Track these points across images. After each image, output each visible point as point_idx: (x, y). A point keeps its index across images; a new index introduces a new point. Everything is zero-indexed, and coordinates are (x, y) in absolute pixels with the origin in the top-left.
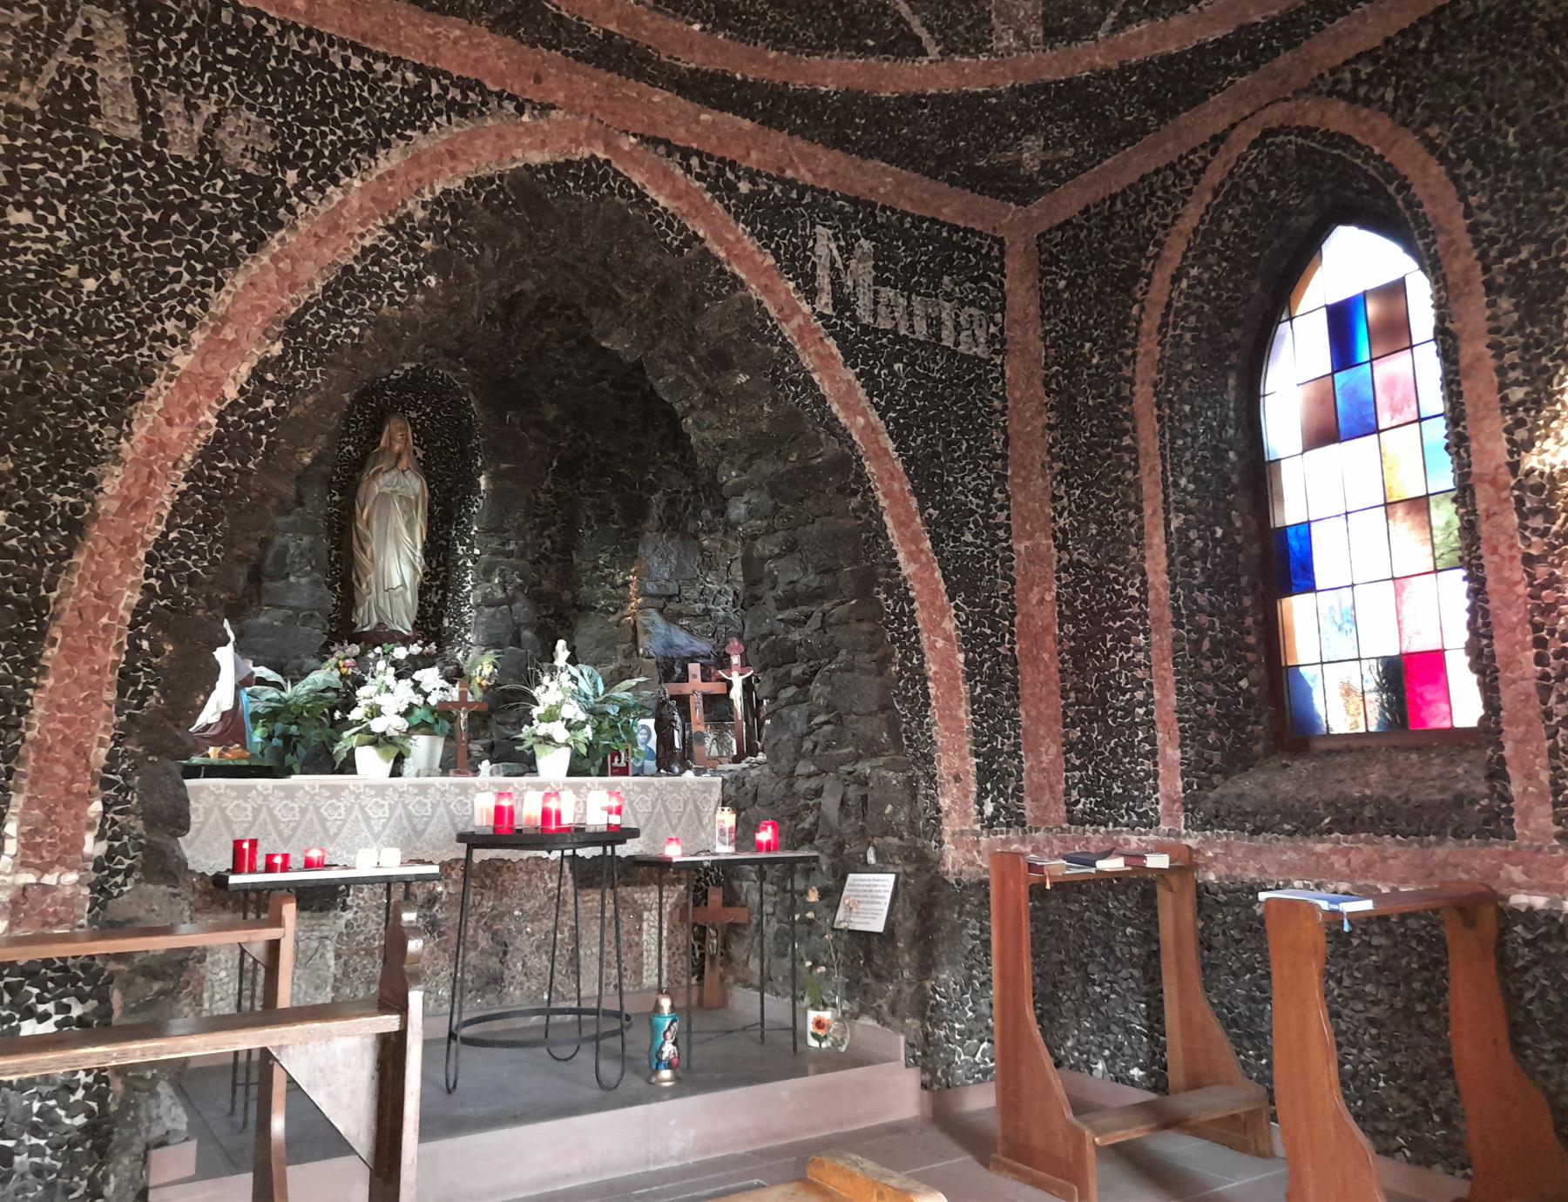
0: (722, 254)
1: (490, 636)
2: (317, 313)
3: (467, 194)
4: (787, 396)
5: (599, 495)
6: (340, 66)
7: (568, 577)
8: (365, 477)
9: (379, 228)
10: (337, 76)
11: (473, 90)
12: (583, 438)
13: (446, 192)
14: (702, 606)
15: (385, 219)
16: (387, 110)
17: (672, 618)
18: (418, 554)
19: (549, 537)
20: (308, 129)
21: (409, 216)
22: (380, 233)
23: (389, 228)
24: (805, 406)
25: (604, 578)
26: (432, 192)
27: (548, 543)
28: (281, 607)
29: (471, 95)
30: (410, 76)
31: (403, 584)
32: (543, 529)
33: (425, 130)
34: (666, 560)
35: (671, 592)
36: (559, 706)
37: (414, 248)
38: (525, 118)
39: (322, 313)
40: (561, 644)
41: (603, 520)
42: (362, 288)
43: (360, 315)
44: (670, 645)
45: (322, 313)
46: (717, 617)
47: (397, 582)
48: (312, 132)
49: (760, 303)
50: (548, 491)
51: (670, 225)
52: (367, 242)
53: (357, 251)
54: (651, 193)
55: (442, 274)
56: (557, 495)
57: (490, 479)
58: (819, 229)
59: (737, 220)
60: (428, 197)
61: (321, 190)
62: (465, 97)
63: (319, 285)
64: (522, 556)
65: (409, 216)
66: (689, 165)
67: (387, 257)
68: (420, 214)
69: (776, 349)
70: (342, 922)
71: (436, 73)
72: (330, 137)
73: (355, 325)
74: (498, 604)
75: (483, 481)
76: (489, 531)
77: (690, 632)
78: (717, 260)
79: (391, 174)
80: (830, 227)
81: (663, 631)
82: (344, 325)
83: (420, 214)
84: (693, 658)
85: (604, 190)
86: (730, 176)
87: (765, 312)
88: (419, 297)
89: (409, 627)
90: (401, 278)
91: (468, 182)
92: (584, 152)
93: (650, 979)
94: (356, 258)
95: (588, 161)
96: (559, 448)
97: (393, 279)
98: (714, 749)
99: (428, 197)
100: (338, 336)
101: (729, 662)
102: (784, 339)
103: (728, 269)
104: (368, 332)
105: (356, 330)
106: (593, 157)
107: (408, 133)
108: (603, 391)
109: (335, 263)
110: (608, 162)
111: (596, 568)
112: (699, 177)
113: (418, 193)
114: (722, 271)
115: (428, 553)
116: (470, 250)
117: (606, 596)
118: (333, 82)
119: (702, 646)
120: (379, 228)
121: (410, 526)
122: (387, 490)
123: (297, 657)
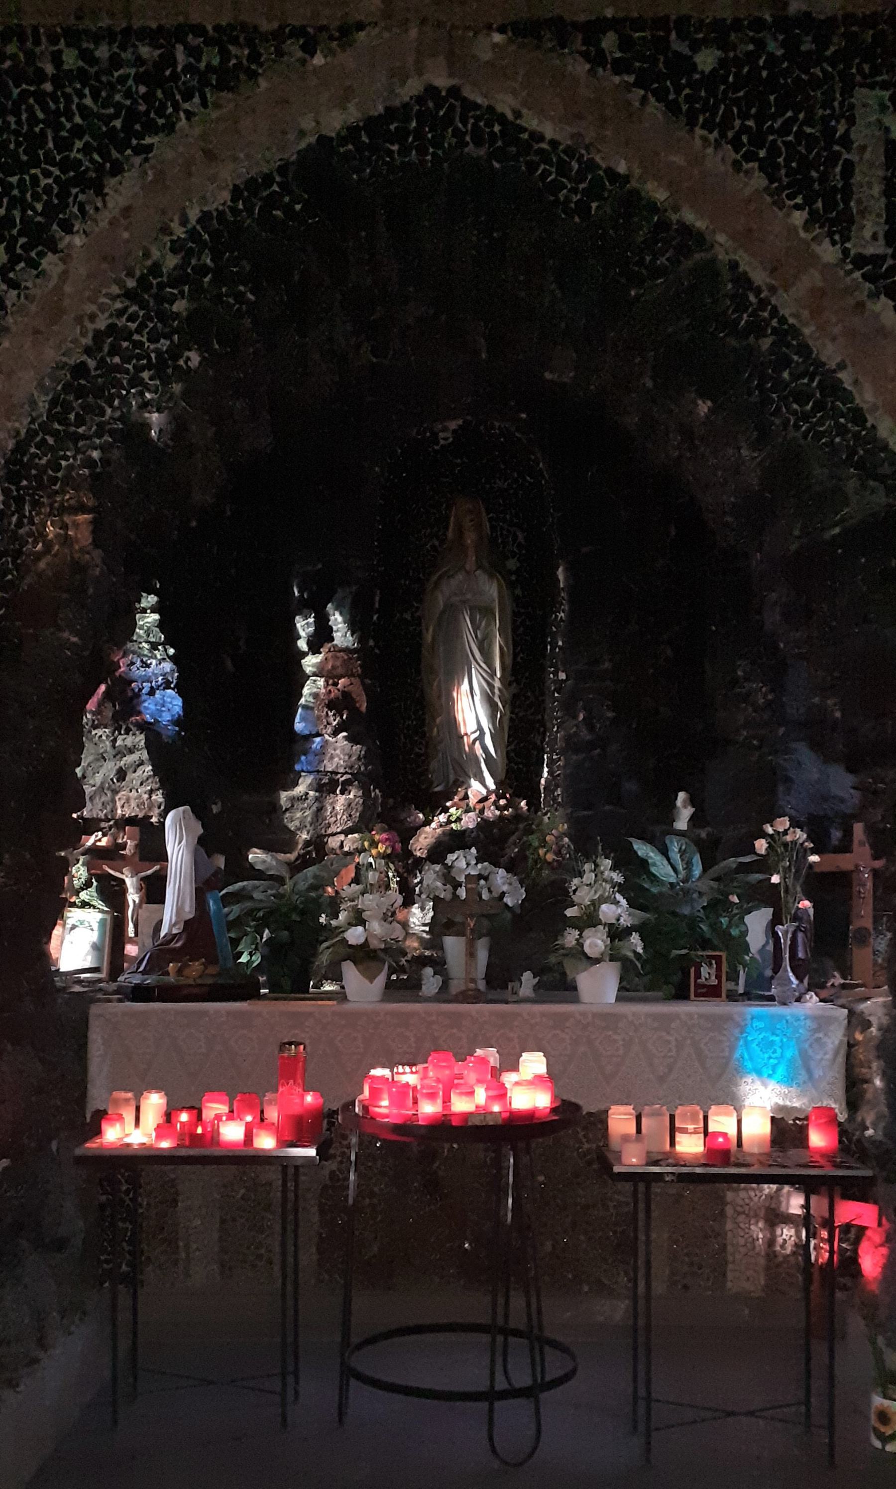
0: (661, 195)
2: (44, 440)
3: (234, 210)
4: (786, 424)
6: (49, 69)
9: (114, 298)
10: (48, 87)
11: (235, 41)
13: (205, 218)
15: (119, 282)
16: (116, 116)
18: (497, 684)
20: (14, 180)
21: (155, 269)
22: (118, 305)
23: (128, 295)
24: (819, 436)
26: (184, 222)
29: (233, 49)
30: (145, 51)
31: (480, 728)
33: (170, 128)
36: (595, 905)
37: (164, 317)
38: (318, 60)
39: (51, 441)
42: (99, 392)
45: (51, 441)
48: (21, 181)
49: (734, 265)
51: (563, 169)
52: (102, 323)
53: (87, 341)
54: (530, 121)
55: (204, 347)
58: (861, 94)
59: (691, 123)
60: (180, 232)
61: (34, 264)
62: (225, 55)
63: (43, 404)
65: (155, 269)
66: (601, 53)
67: (128, 338)
68: (172, 261)
69: (766, 343)
70: (326, 1172)
71: (179, 33)
72: (44, 182)
75: (561, 573)
78: (653, 207)
79: (127, 211)
80: (884, 86)
82: (78, 451)
83: (172, 261)
85: (450, 140)
86: (680, 47)
87: (743, 281)
88: (177, 388)
90: (149, 366)
91: (236, 193)
92: (413, 87)
94: (88, 351)
95: (420, 100)
97: (139, 369)
99: (180, 232)
100: (71, 467)
102: (783, 320)
103: (674, 217)
104: (116, 454)
105: (96, 454)
106: (431, 91)
107: (148, 140)
109: (61, 366)
110: (454, 91)
112: (619, 67)
113: (165, 230)
114: (663, 225)
116: (240, 297)
118: (40, 97)
120: (114, 298)
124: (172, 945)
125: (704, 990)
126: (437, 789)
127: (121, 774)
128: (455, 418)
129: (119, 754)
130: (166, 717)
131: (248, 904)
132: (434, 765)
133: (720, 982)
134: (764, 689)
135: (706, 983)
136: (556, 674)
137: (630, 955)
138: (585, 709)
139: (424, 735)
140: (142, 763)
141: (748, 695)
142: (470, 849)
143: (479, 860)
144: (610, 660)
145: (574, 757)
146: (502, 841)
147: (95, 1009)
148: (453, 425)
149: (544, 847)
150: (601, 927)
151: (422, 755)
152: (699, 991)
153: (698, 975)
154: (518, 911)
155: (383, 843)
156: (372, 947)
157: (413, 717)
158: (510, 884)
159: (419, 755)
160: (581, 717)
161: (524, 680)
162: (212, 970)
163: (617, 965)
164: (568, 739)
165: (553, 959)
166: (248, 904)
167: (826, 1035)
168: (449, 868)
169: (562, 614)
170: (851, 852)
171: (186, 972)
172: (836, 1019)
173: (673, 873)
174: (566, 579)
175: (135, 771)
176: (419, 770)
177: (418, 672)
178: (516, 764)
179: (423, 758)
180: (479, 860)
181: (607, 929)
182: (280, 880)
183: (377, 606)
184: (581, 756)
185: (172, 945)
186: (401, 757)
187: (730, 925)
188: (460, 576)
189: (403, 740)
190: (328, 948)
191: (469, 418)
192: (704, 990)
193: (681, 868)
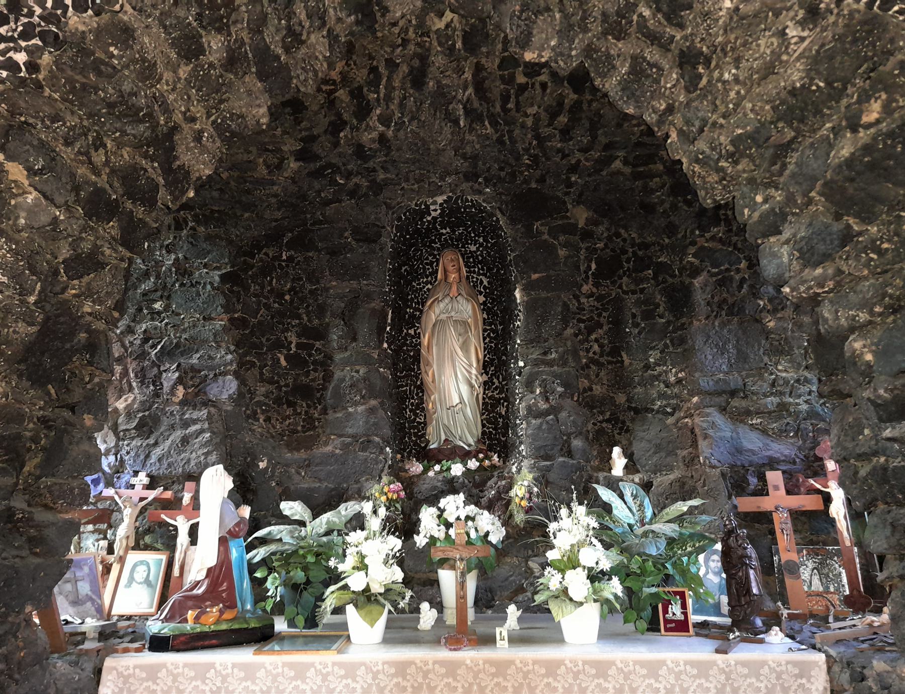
1: (538, 449)
5: (642, 291)
7: (621, 381)
12: (618, 235)
14: (775, 400)
17: (739, 417)
18: (474, 371)
19: (596, 340)
25: (657, 378)
27: (596, 347)
28: (340, 436)
31: (462, 401)
32: (590, 333)
34: (723, 351)
35: (732, 386)
40: (617, 451)
41: (648, 315)
43: (26, 34)
44: (739, 450)
46: (797, 414)
47: (456, 400)
50: (591, 295)
56: (599, 298)
57: (525, 290)
64: (565, 364)
73: (17, 49)
74: (546, 413)
75: (518, 294)
76: (531, 341)
77: (764, 432)
81: (728, 434)
84: (772, 464)
89: (471, 441)
93: (848, 543)
96: (596, 250)
98: (816, 581)
101: (823, 467)
105: (21, 58)
108: (619, 172)
111: (647, 367)
115: (485, 367)
117: (662, 396)
119: (782, 449)
121: (465, 347)
122: (443, 317)
123: (357, 482)
124: (195, 592)
125: (673, 625)
127: (185, 440)
128: (441, 194)
129: (186, 424)
130: (225, 396)
131: (273, 547)
132: (430, 429)
133: (685, 614)
134: (674, 370)
135: (673, 618)
136: (516, 362)
137: (611, 597)
138: (540, 386)
139: (423, 409)
140: (202, 431)
141: (660, 375)
143: (466, 503)
144: (556, 352)
145: (534, 421)
146: (481, 486)
147: (109, 662)
148: (440, 199)
150: (579, 570)
152: (669, 626)
153: (666, 611)
154: (500, 546)
156: (373, 591)
158: (493, 524)
159: (419, 423)
160: (538, 391)
162: (228, 615)
163: (598, 605)
164: (529, 408)
165: (539, 598)
166: (273, 547)
167: (809, 681)
168: (442, 511)
170: (767, 494)
171: (203, 619)
172: (815, 663)
173: (630, 515)
174: (521, 298)
175: (196, 438)
178: (488, 428)
180: (466, 503)
181: (586, 571)
182: (302, 524)
183: (389, 321)
184: (539, 421)
185: (195, 592)
187: (688, 564)
188: (447, 301)
190: (333, 592)
192: (673, 625)
193: (635, 511)
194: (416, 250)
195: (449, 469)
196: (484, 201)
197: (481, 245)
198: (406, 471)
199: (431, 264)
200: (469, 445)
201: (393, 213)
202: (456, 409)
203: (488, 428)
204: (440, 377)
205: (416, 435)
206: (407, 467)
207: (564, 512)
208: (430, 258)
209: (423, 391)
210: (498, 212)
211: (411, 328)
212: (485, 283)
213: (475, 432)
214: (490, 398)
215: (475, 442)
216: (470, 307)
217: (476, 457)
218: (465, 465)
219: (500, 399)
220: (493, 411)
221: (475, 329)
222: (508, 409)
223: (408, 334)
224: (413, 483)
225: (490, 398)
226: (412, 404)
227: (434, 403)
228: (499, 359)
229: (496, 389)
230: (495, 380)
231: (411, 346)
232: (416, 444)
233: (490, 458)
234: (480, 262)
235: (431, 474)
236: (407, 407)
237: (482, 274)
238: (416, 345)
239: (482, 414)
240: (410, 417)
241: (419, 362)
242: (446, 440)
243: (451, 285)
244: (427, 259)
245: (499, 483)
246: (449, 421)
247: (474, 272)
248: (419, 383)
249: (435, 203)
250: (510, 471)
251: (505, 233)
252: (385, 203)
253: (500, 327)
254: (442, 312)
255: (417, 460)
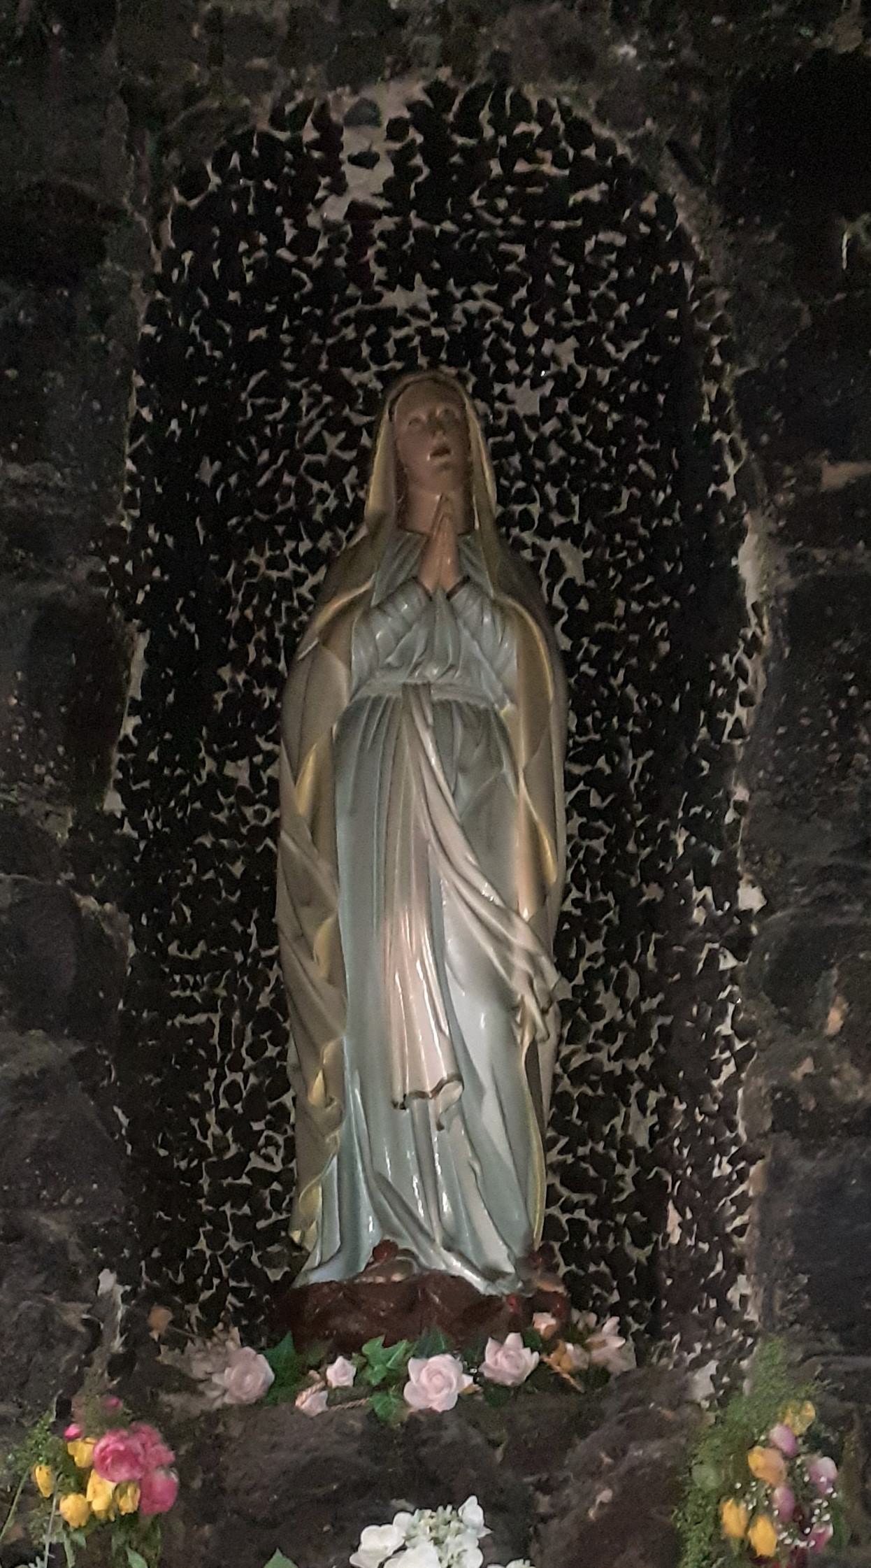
8: (308, 645)
18: (522, 938)
89: (500, 1255)
122: (388, 684)
126: (316, 1277)
128: (403, 68)
142: (457, 1503)
145: (804, 1166)
149: (739, 1495)
151: (275, 1177)
155: (105, 1472)
157: (249, 1062)
159: (262, 1178)
160: (835, 1020)
161: (584, 965)
169: (741, 712)
174: (765, 576)
176: (261, 1224)
177: (270, 934)
178: (568, 1207)
179: (276, 1186)
186: (205, 1182)
189: (215, 1129)
191: (444, 73)
194: (271, 388)
195: (399, 1378)
196: (602, 113)
197: (564, 383)
198: (191, 1386)
199: (334, 472)
200: (491, 1274)
201: (165, 146)
202: (435, 1106)
203: (568, 1207)
204: (364, 955)
205: (244, 1228)
206: (199, 1369)
207: (440, 1509)
208: (332, 442)
209: (280, 1038)
210: (668, 163)
211: (235, 756)
212: (574, 566)
213: (517, 1215)
214: (578, 1076)
215: (518, 1263)
216: (509, 649)
217: (522, 1324)
218: (472, 1360)
219: (627, 1076)
220: (593, 1135)
221: (533, 747)
222: (664, 1122)
223: (228, 785)
224: (220, 1443)
225: (578, 1076)
226: (233, 1092)
227: (335, 1082)
228: (626, 898)
229: (609, 1034)
230: (606, 999)
231: (234, 834)
232: (242, 1268)
233: (579, 1337)
234: (553, 474)
235: (309, 1401)
236: (209, 1101)
237: (562, 532)
238: (258, 834)
239: (548, 1145)
240: (221, 1147)
241: (269, 904)
242: (384, 1249)
243: (426, 544)
244: (318, 445)
245: (636, 1453)
246: (398, 1162)
247: (525, 521)
248: (264, 1000)
249: (365, 116)
250: (681, 1397)
251: (701, 268)
252: (128, 94)
253: (634, 763)
254: (377, 666)
255: (248, 1339)
